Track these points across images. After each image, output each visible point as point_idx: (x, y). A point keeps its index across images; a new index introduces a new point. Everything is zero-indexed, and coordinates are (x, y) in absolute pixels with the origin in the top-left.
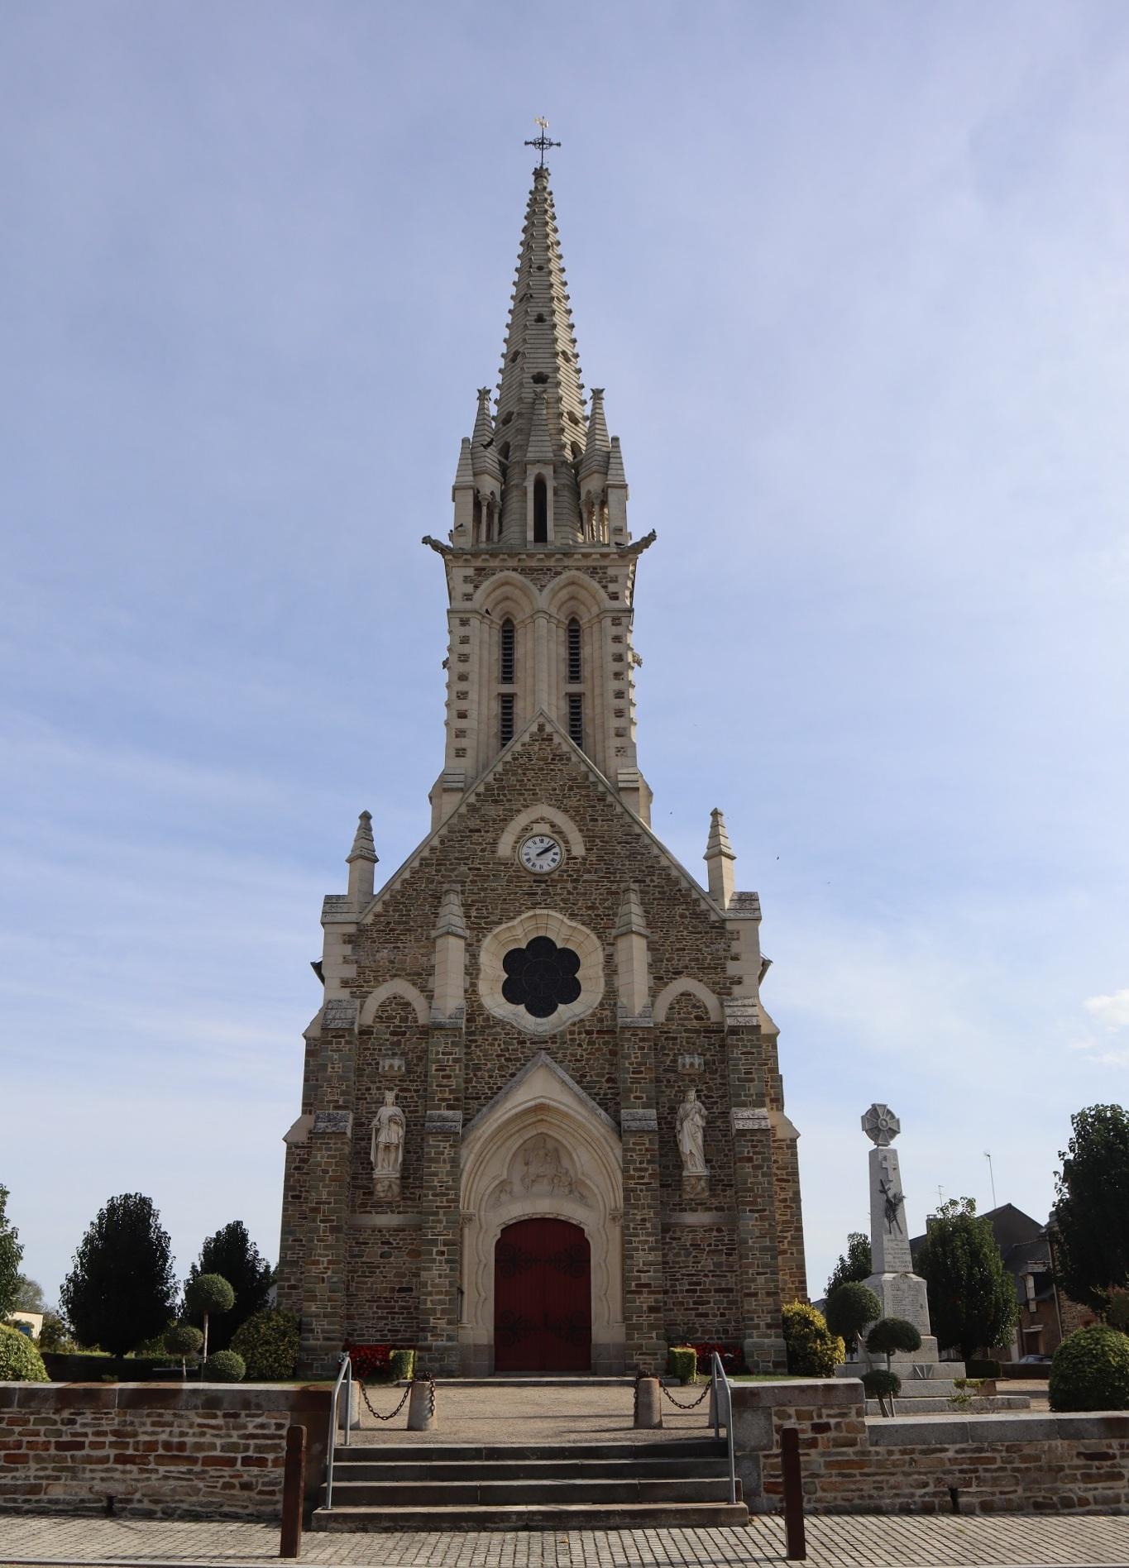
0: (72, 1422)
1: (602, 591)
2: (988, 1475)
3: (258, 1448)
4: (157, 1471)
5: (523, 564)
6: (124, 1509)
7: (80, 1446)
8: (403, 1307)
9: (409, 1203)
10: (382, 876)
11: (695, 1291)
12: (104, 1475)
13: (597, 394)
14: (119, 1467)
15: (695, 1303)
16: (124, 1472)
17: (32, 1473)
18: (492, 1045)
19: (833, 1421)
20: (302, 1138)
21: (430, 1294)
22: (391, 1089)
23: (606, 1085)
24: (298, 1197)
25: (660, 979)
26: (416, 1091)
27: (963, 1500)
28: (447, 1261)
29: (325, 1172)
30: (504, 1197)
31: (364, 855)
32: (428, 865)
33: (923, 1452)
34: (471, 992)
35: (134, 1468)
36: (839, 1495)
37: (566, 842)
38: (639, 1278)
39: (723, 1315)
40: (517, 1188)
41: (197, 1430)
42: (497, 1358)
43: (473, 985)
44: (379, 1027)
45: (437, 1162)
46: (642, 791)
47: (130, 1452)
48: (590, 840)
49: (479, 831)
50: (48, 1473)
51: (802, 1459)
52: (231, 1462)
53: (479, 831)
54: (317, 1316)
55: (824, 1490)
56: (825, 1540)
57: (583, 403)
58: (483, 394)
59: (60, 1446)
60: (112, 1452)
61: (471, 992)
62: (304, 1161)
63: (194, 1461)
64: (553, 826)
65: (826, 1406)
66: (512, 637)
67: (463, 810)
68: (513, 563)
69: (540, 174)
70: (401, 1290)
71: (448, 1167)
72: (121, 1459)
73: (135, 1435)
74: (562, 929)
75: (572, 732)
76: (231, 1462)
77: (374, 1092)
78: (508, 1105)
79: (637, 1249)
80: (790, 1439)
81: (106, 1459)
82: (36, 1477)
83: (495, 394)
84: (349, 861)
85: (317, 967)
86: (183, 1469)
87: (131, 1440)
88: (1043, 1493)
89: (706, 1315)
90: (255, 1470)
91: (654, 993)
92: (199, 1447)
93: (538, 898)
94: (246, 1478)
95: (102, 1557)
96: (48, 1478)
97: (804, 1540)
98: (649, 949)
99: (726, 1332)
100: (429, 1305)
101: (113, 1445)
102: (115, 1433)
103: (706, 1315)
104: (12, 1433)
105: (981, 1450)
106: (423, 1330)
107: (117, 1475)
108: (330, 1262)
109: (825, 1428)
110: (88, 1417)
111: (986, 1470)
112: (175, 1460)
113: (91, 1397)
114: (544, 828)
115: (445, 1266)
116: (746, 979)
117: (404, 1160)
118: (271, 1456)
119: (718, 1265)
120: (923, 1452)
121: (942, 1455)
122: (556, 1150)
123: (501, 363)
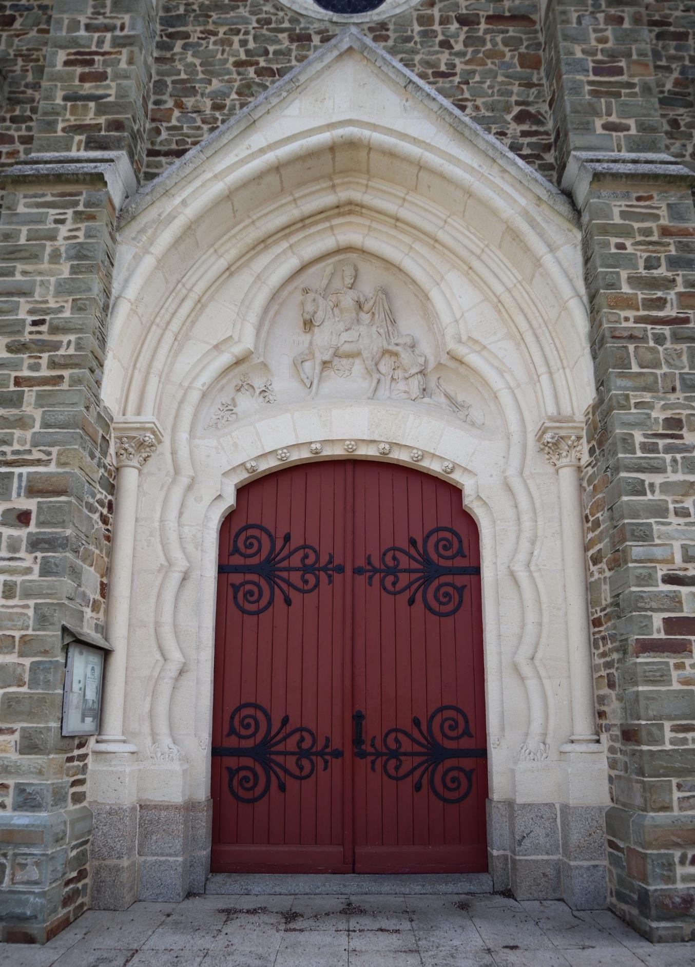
18: (228, 43)
28: (35, 544)
30: (246, 403)
40: (283, 382)
42: (218, 833)
45: (34, 257)
71: (65, 270)
78: (257, 140)
79: (660, 511)
115: (27, 559)
122: (385, 292)
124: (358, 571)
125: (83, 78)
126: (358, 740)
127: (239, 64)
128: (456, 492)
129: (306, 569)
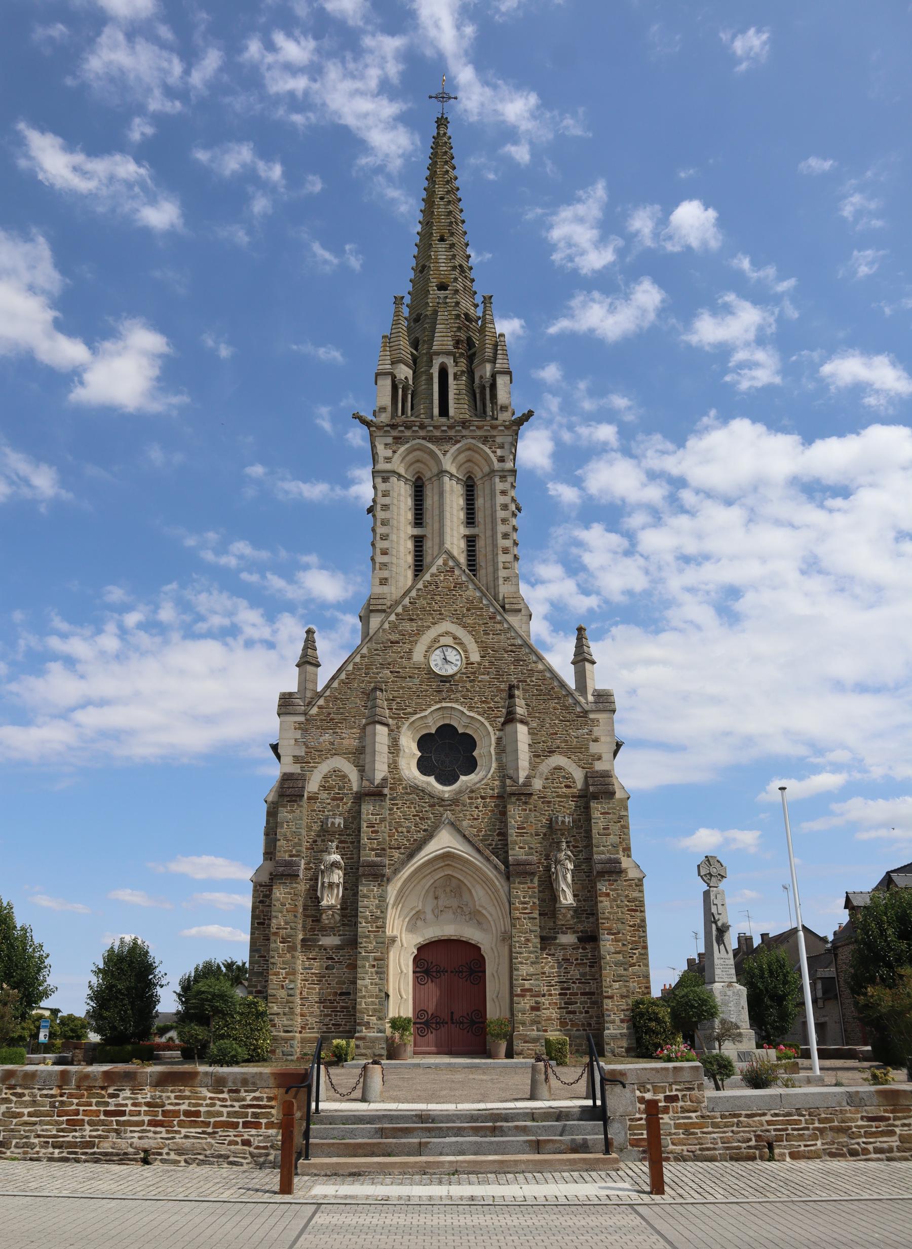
0: (115, 1096)
1: (492, 455)
2: (795, 1133)
3: (255, 1115)
4: (179, 1132)
5: (430, 434)
6: (156, 1159)
7: (123, 1113)
8: (342, 1007)
9: (347, 928)
10: (323, 675)
11: (566, 994)
12: (141, 1135)
13: (487, 300)
14: (152, 1129)
15: (565, 1003)
16: (155, 1133)
17: (87, 1133)
19: (680, 1094)
20: (265, 878)
21: (364, 997)
22: (332, 841)
23: (496, 838)
24: (263, 924)
25: (538, 755)
26: (352, 843)
27: (777, 1151)
28: (377, 973)
29: (283, 905)
30: (419, 923)
31: (308, 660)
32: (359, 669)
33: (748, 1116)
34: (394, 767)
35: (163, 1129)
36: (685, 1148)
37: (465, 651)
38: (523, 985)
39: (587, 1012)
41: (208, 1101)
43: (395, 762)
44: (324, 795)
45: (368, 897)
46: (523, 612)
47: (160, 1118)
48: (484, 648)
49: (398, 642)
50: (99, 1133)
51: (661, 1121)
52: (235, 1126)
53: (398, 642)
54: (278, 1014)
55: (673, 1144)
56: (676, 1179)
57: (476, 306)
58: (398, 301)
59: (107, 1113)
60: (146, 1119)
61: (394, 767)
62: (266, 896)
63: (207, 1124)
64: (455, 638)
65: (676, 1083)
66: (421, 491)
67: (386, 626)
68: (422, 433)
69: (442, 122)
70: (342, 994)
72: (152, 1123)
73: (163, 1106)
74: (464, 716)
75: (469, 565)
76: (235, 1126)
77: (319, 843)
80: (652, 1108)
81: (142, 1123)
82: (90, 1137)
83: (407, 300)
84: (298, 666)
85: (275, 748)
86: (199, 1130)
87: (160, 1109)
88: (836, 1146)
89: (574, 1012)
90: (253, 1132)
91: (533, 767)
92: (209, 1114)
93: (444, 694)
94: (246, 1137)
95: (198, 1196)
96: (99, 1137)
97: (663, 1181)
98: (529, 733)
99: (589, 1025)
100: (364, 1006)
101: (146, 1113)
102: (148, 1104)
103: (574, 1012)
104: (72, 1104)
105: (789, 1114)
106: (360, 1024)
107: (150, 1135)
108: (287, 974)
109: (674, 1099)
110: (127, 1093)
111: (793, 1129)
112: (194, 1124)
113: (129, 1077)
114: (449, 640)
116: (605, 757)
117: (343, 896)
118: (264, 1121)
119: (583, 975)
120: (748, 1116)
121: (762, 1118)
123: (412, 275)
124: (452, 972)
125: (372, 832)
126: (452, 1019)
127: (414, 816)
128: (479, 949)
129: (438, 972)
